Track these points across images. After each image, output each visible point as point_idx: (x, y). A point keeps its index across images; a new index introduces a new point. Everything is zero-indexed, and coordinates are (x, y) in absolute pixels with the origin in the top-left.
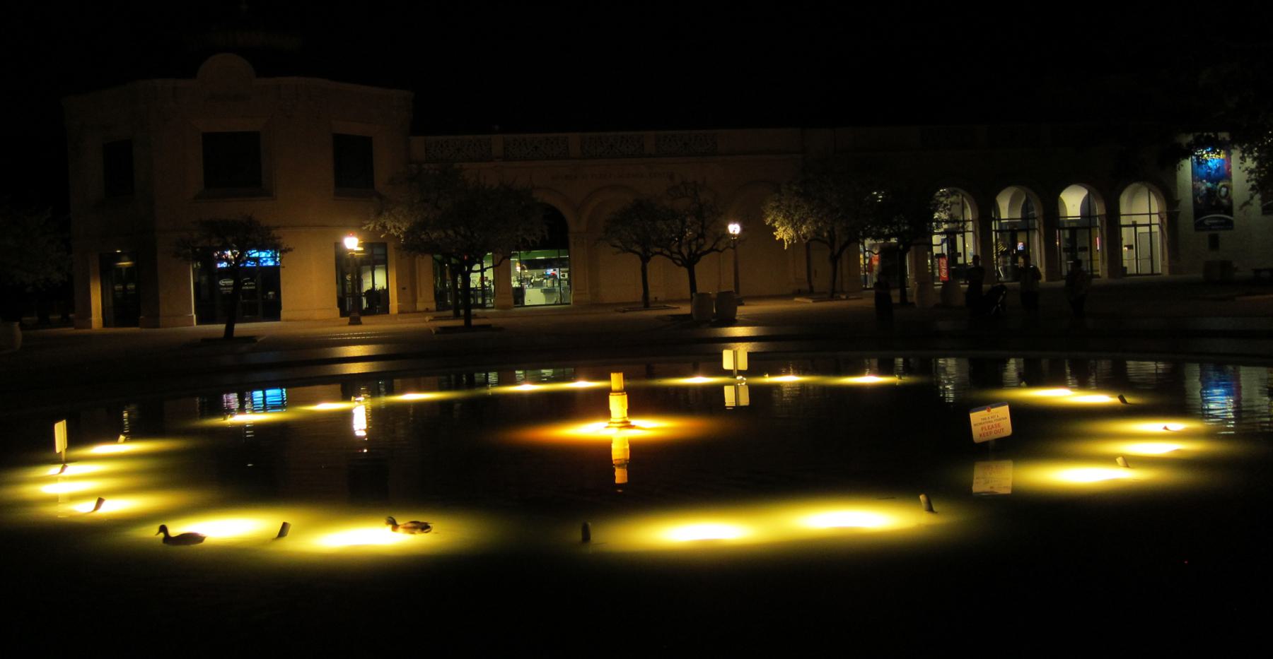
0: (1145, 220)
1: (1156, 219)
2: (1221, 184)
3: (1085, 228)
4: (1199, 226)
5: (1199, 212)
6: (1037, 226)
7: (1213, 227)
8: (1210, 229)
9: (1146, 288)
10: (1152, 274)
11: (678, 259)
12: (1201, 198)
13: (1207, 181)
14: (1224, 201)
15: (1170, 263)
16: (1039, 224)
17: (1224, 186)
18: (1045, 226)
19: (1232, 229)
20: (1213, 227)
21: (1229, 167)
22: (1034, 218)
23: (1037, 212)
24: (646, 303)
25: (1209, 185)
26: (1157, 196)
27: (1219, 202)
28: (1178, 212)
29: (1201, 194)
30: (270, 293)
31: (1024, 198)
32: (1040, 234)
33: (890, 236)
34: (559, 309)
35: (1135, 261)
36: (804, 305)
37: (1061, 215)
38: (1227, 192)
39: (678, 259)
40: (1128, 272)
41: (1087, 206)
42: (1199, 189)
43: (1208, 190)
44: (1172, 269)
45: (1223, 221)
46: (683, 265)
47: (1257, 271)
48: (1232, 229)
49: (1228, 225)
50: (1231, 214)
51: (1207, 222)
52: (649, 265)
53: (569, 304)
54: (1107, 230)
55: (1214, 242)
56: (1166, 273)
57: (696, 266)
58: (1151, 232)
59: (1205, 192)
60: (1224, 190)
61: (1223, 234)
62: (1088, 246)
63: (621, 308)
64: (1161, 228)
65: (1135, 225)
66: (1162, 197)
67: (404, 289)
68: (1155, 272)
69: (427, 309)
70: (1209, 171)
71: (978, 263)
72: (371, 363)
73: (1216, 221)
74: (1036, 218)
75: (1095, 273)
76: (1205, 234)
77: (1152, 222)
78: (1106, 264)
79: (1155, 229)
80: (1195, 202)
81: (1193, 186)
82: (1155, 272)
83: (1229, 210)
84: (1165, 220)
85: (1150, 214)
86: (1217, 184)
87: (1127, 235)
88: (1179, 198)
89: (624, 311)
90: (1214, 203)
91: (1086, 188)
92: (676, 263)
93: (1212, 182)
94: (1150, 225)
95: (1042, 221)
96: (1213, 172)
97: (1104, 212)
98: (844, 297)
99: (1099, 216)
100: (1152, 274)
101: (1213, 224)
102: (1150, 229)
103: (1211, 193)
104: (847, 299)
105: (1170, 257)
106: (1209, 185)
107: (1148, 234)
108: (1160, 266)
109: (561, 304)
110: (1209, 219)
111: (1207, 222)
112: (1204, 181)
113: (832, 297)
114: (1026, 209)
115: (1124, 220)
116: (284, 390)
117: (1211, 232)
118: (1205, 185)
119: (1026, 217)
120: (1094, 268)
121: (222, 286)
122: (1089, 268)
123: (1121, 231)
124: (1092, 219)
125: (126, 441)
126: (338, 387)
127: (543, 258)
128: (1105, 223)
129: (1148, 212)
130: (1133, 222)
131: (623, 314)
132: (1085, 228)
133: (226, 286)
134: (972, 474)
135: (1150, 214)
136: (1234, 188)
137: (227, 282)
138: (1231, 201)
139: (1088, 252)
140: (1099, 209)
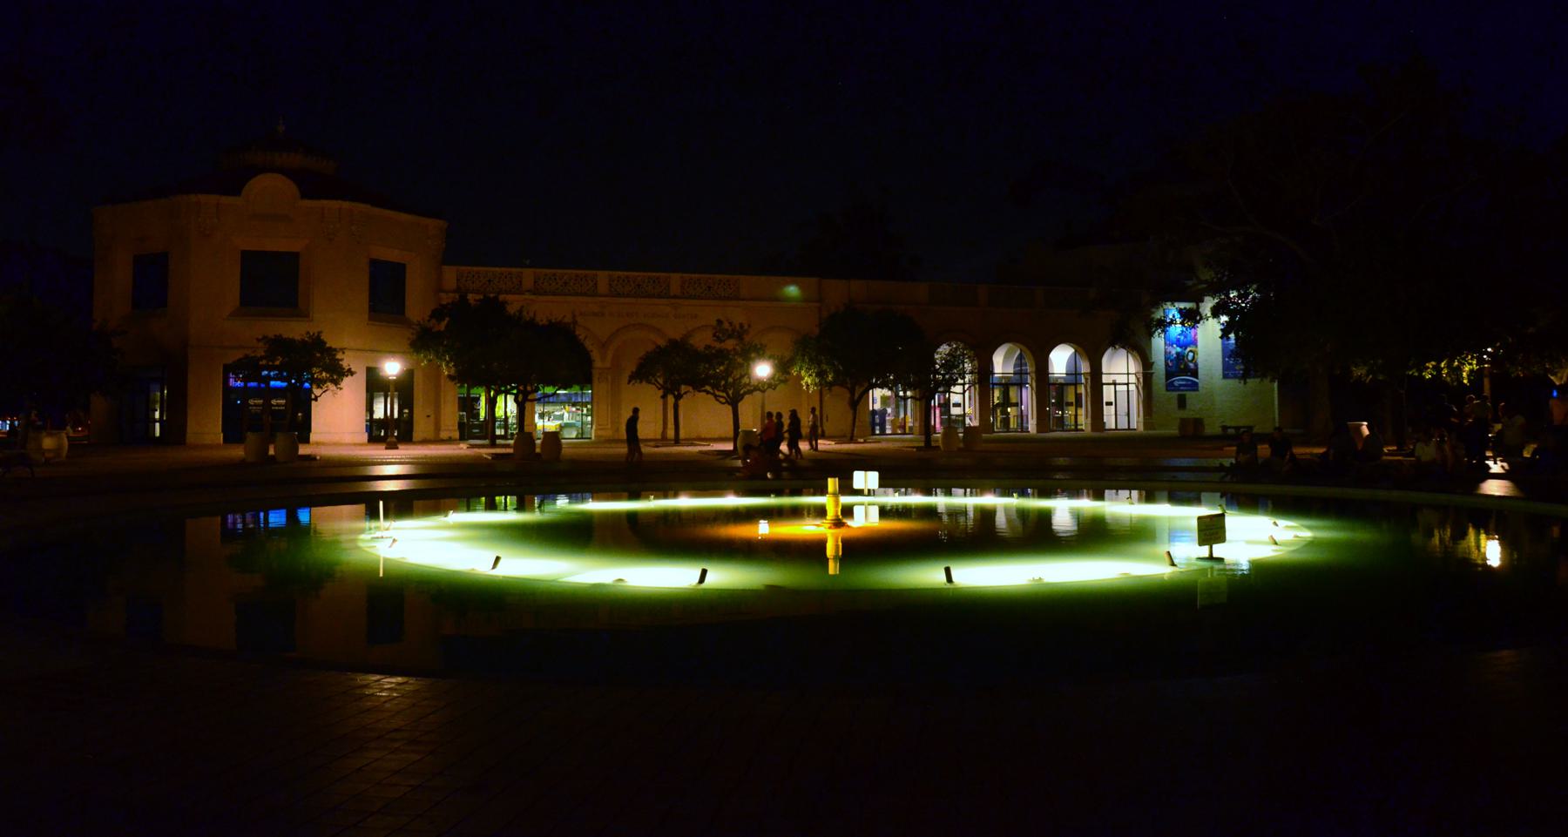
0: (1123, 379)
1: (1133, 379)
2: (1188, 349)
3: (1071, 384)
4: (1170, 387)
5: (1170, 374)
8: (1179, 390)
9: (1125, 441)
11: (722, 397)
14: (1191, 365)
16: (1032, 379)
17: (1191, 351)
18: (1037, 381)
19: (1197, 390)
22: (1027, 374)
23: (1030, 368)
24: (677, 441)
25: (1179, 349)
26: (1134, 356)
27: (1187, 366)
29: (1172, 358)
30: (300, 414)
31: (1018, 352)
32: (1032, 389)
34: (582, 443)
35: (1114, 417)
36: (897, 445)
37: (1050, 371)
38: (1194, 357)
39: (722, 397)
40: (1107, 427)
41: (1073, 363)
42: (1170, 352)
44: (1147, 425)
46: (727, 402)
47: (1225, 428)
49: (1194, 386)
50: (1197, 377)
51: (1176, 384)
52: (681, 402)
53: (590, 438)
54: (1091, 387)
55: (1182, 402)
56: (1141, 428)
57: (740, 404)
58: (1128, 391)
59: (1175, 356)
60: (1191, 354)
61: (1189, 394)
62: (1113, 400)
63: (652, 444)
64: (1137, 387)
65: (1115, 384)
66: (1138, 358)
67: (428, 416)
68: (1131, 427)
69: (450, 438)
71: (255, 397)
72: (361, 490)
73: (1184, 383)
75: (1079, 427)
76: (1175, 394)
78: (1089, 419)
79: (1132, 387)
80: (1167, 365)
81: (1166, 352)
82: (1131, 427)
83: (1195, 373)
84: (1141, 380)
85: (1128, 374)
86: (1186, 348)
87: (1108, 393)
88: (1153, 361)
89: (657, 447)
90: (1182, 366)
91: (1072, 347)
92: (718, 400)
94: (1128, 384)
95: (1034, 375)
97: (1089, 371)
98: (862, 440)
99: (1084, 374)
100: (1129, 429)
101: (1181, 385)
102: (1021, 377)
103: (1180, 357)
104: (865, 442)
105: (1145, 415)
106: (1179, 349)
108: (1137, 422)
109: (582, 438)
110: (1178, 380)
111: (1176, 384)
112: (1175, 346)
113: (852, 440)
114: (1020, 361)
115: (1105, 379)
118: (1175, 350)
119: (1020, 373)
120: (1079, 422)
121: (251, 406)
124: (1078, 376)
125: (654, 499)
126: (361, 508)
128: (1089, 381)
131: (656, 449)
132: (1071, 384)
133: (255, 405)
135: (1128, 374)
136: (1199, 352)
137: (278, 401)
138: (1196, 365)
139: (1113, 407)
140: (1085, 367)
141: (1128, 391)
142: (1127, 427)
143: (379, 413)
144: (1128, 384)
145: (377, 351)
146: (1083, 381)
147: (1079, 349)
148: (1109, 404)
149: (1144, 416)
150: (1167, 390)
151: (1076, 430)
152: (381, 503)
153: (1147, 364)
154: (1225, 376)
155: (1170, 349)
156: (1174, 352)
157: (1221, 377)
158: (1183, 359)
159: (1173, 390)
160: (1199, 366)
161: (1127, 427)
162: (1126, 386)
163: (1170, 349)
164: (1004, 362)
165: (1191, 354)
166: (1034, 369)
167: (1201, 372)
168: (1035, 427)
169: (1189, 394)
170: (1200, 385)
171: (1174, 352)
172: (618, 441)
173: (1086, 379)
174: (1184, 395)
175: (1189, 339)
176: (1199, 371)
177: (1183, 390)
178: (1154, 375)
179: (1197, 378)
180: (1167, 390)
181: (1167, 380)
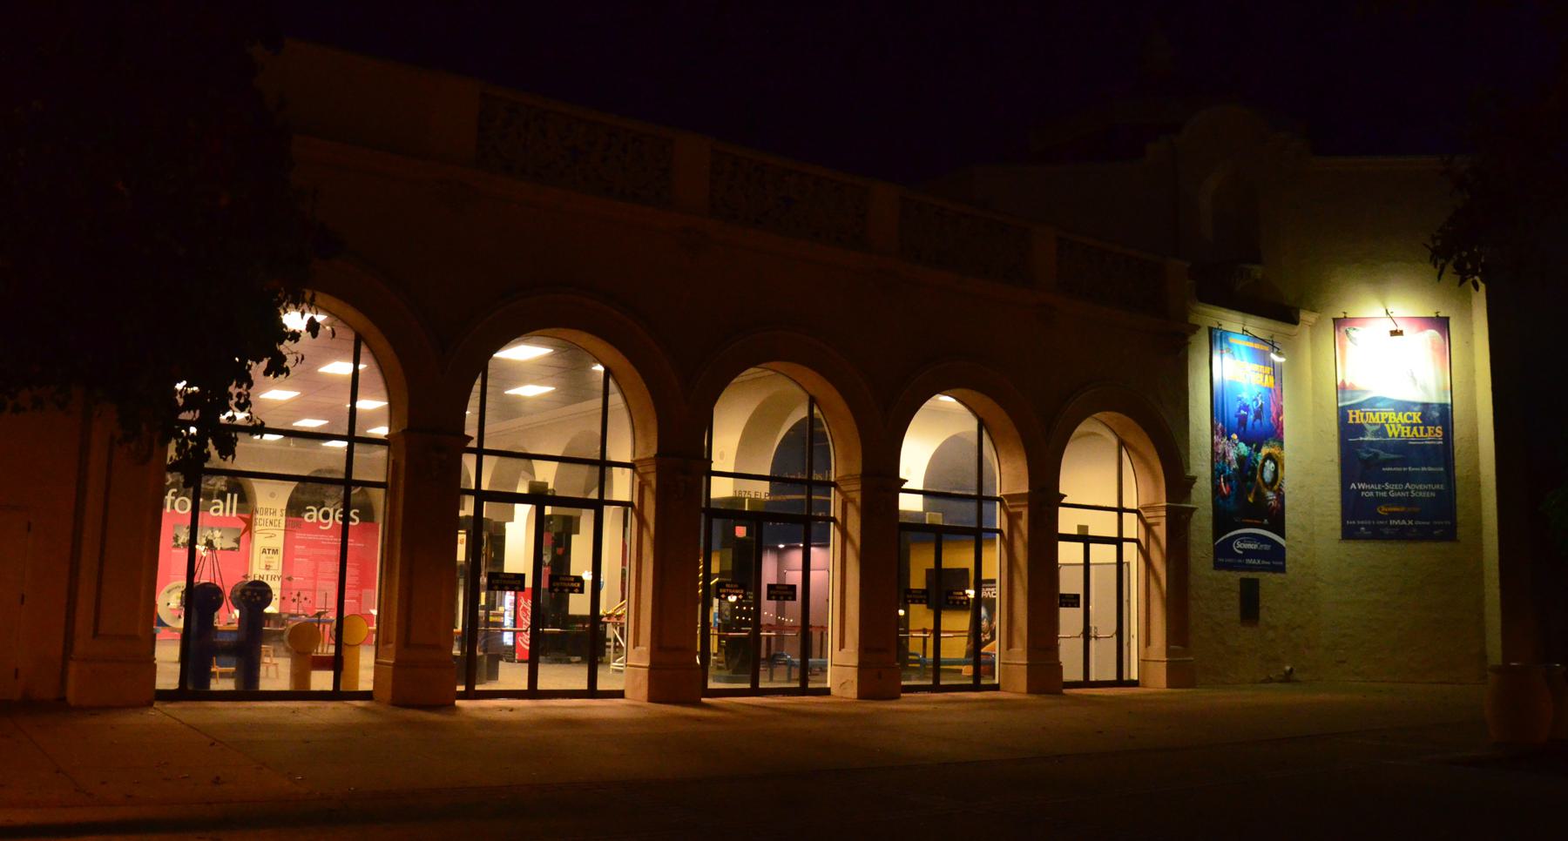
0: (1103, 525)
2: (1265, 450)
4: (1224, 556)
5: (1223, 521)
6: (835, 510)
7: (1249, 561)
10: (1120, 682)
12: (1227, 479)
13: (1241, 440)
15: (1169, 653)
17: (1269, 457)
19: (1282, 569)
20: (1249, 561)
21: (1280, 413)
25: (1243, 448)
27: (1260, 497)
28: (1193, 510)
32: (845, 536)
33: (212, 399)
38: (1276, 473)
43: (1241, 460)
44: (1179, 674)
45: (1267, 547)
48: (1282, 569)
49: (1275, 557)
50: (1279, 528)
51: (1238, 546)
56: (1158, 679)
58: (1087, 564)
59: (1235, 466)
60: (1270, 466)
61: (1268, 581)
62: (1081, 592)
70: (1243, 412)
74: (835, 485)
76: (1234, 577)
77: (1125, 536)
80: (1216, 489)
81: (1214, 453)
83: (1276, 520)
86: (1258, 450)
88: (1192, 473)
93: (1248, 444)
94: (1118, 541)
96: (1251, 417)
107: (1082, 568)
110: (1245, 537)
111: (1238, 546)
112: (1235, 436)
115: (1068, 521)
116: (1441, 443)
117: (1245, 575)
122: (930, 655)
123: (507, 574)
124: (985, 505)
127: (700, 606)
128: (1023, 524)
129: (1115, 504)
130: (1080, 527)
134: (359, 650)
135: (1120, 510)
138: (1281, 497)
139: (1080, 611)
141: (1087, 564)
142: (1112, 676)
143: (228, 685)
144: (1118, 541)
145: (191, 727)
146: (1000, 520)
147: (1000, 417)
148: (1072, 601)
149: (1169, 642)
150: (1218, 566)
151: (1120, 682)
152: (1384, 469)
153: (1177, 482)
154: (1348, 533)
155: (1223, 444)
156: (1232, 455)
157: (1339, 534)
158: (1253, 479)
159: (1229, 567)
160: (1287, 503)
161: (1112, 676)
162: (1114, 547)
163: (1223, 444)
164: (741, 443)
165: (1270, 466)
166: (857, 468)
167: (1290, 517)
168: (852, 675)
169: (1268, 581)
170: (1289, 555)
171: (1232, 455)
172: (965, 631)
173: (1012, 519)
174: (1256, 582)
175: (1265, 419)
176: (1288, 515)
177: (1251, 568)
178: (1195, 515)
179: (1282, 535)
180: (1218, 566)
181: (1216, 536)
